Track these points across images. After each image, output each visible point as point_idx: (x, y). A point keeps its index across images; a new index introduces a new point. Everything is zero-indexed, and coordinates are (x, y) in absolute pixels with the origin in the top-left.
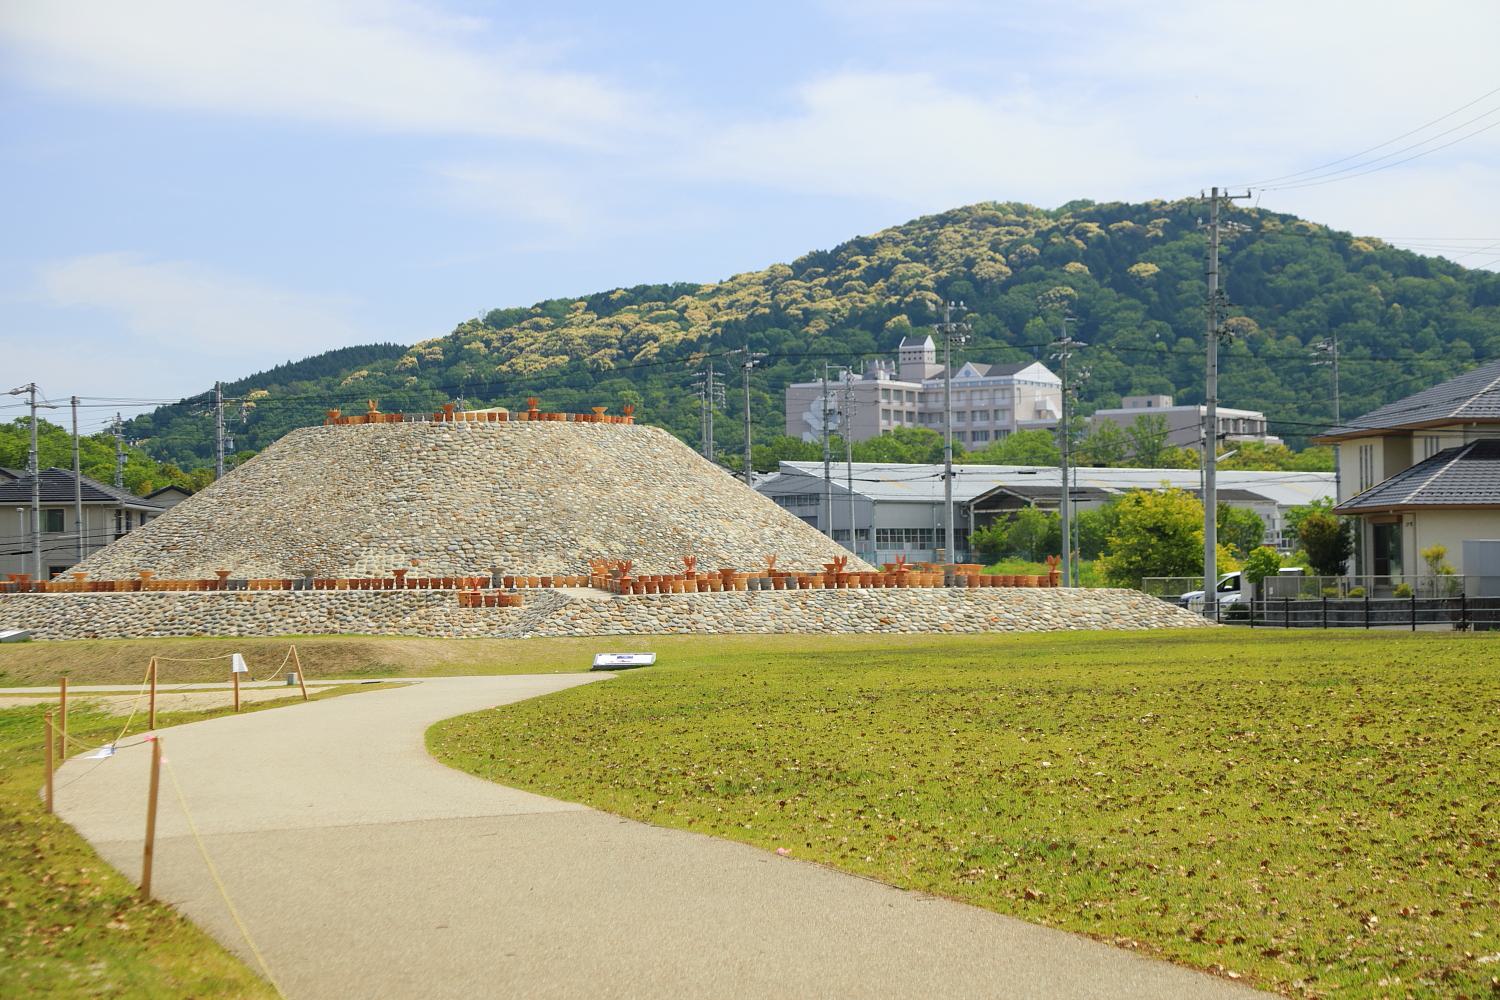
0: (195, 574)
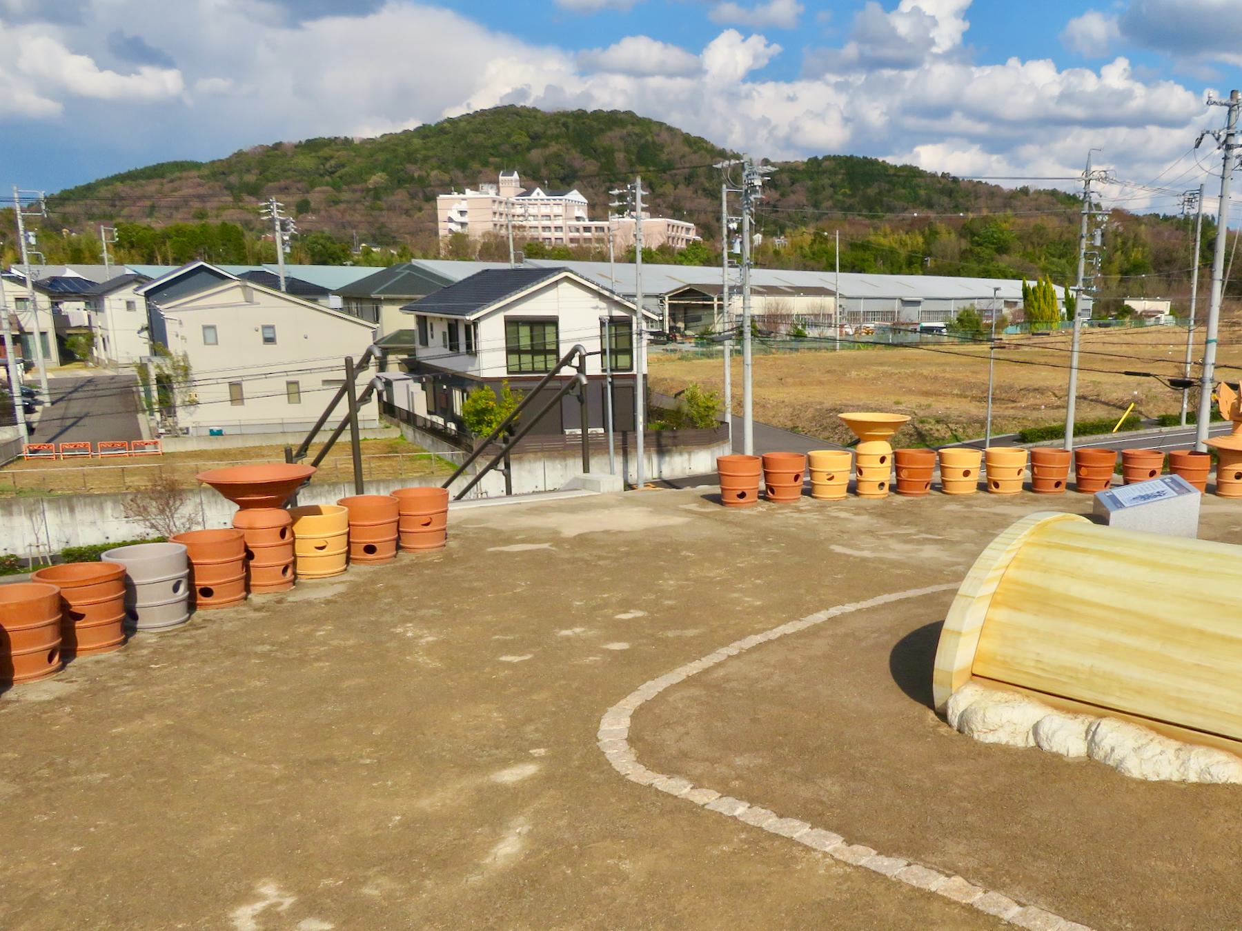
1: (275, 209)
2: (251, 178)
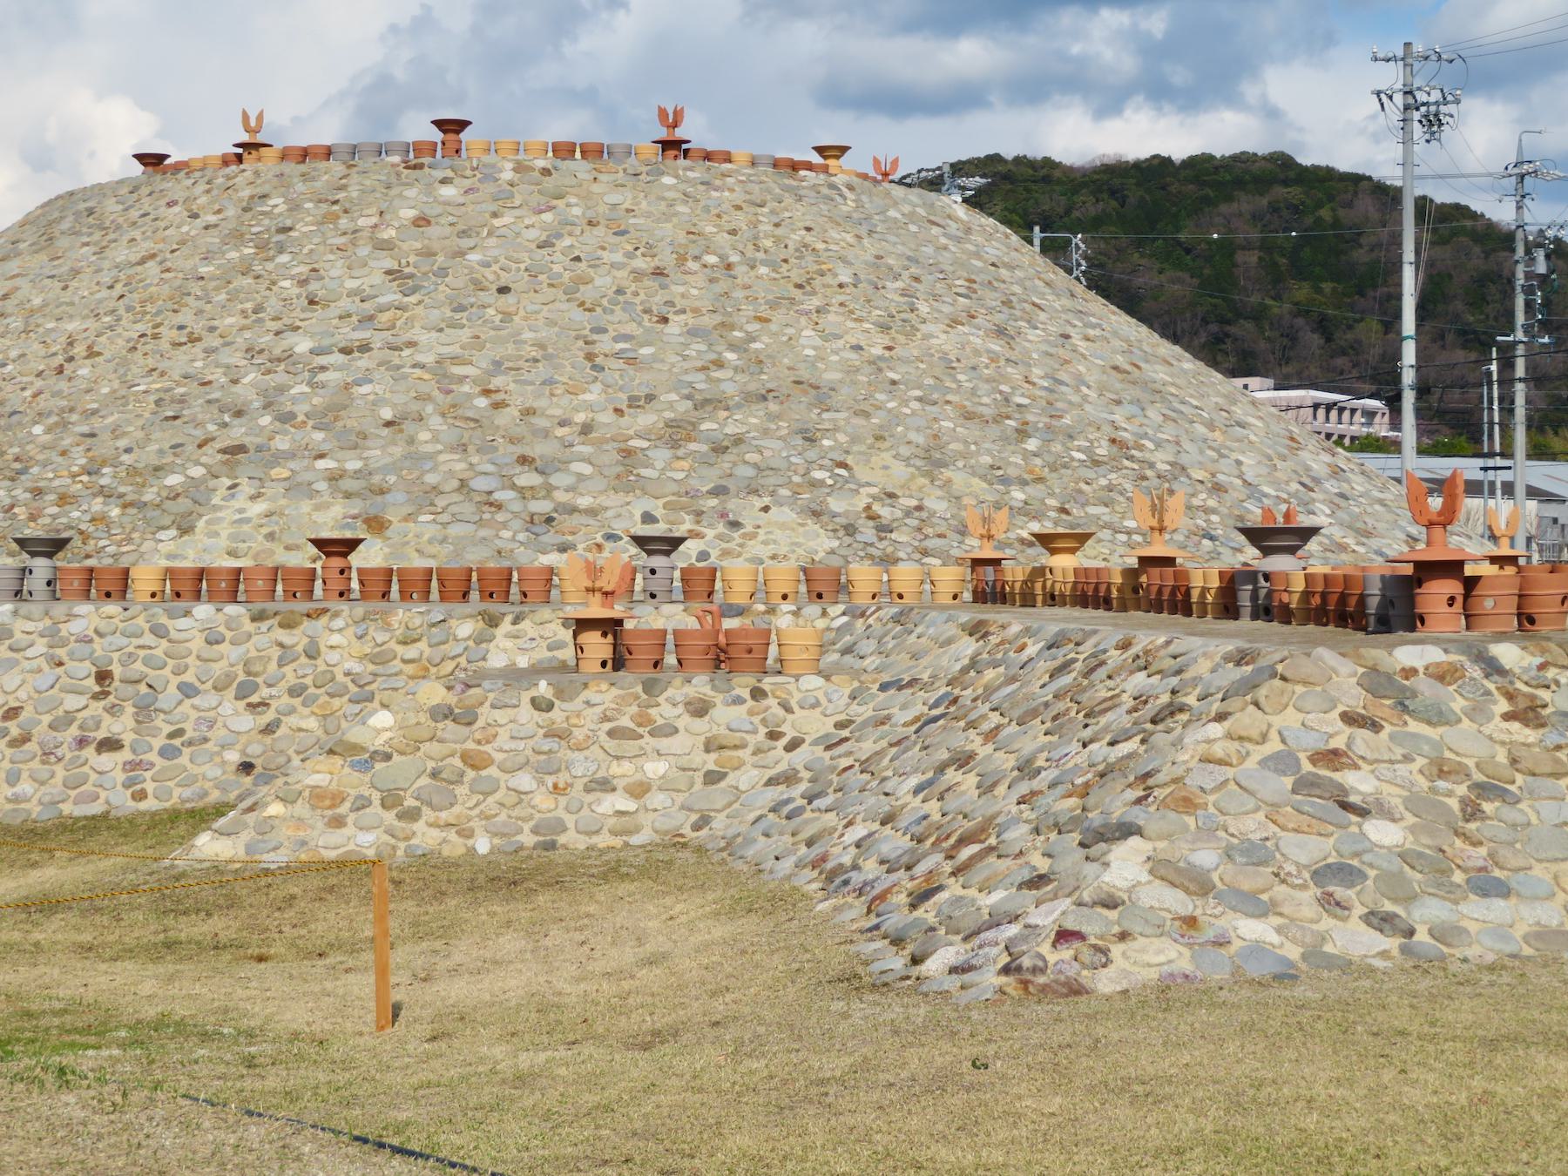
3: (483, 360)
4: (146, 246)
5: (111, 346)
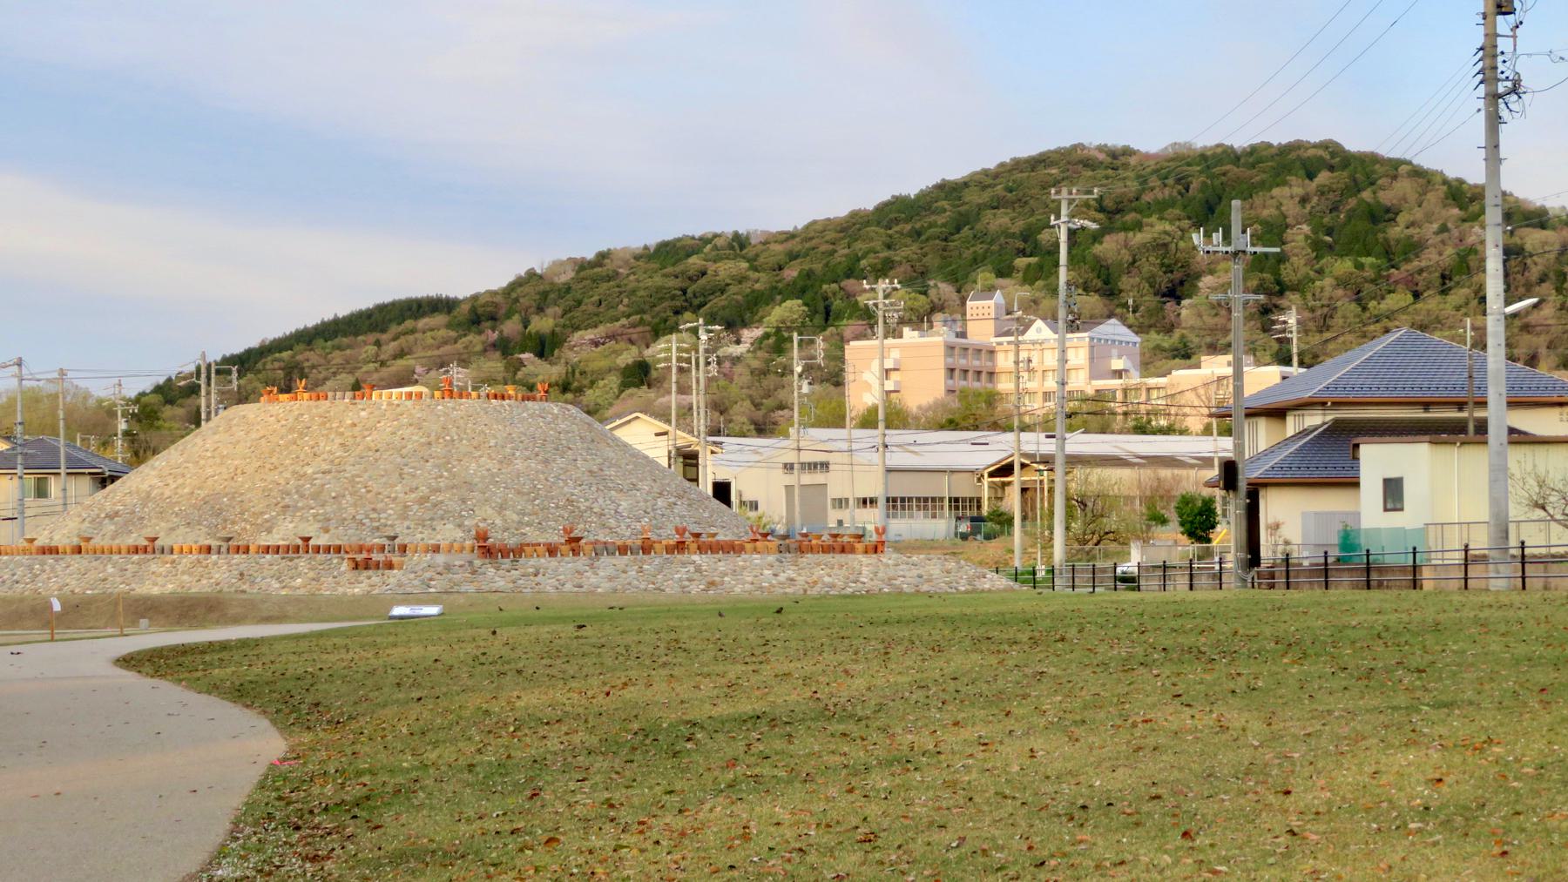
0: (131, 540)
1: (795, 335)
2: (543, 324)
3: (366, 476)
4: (262, 433)
5: (250, 470)
